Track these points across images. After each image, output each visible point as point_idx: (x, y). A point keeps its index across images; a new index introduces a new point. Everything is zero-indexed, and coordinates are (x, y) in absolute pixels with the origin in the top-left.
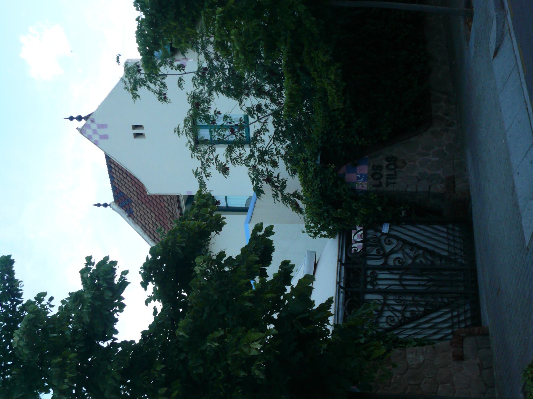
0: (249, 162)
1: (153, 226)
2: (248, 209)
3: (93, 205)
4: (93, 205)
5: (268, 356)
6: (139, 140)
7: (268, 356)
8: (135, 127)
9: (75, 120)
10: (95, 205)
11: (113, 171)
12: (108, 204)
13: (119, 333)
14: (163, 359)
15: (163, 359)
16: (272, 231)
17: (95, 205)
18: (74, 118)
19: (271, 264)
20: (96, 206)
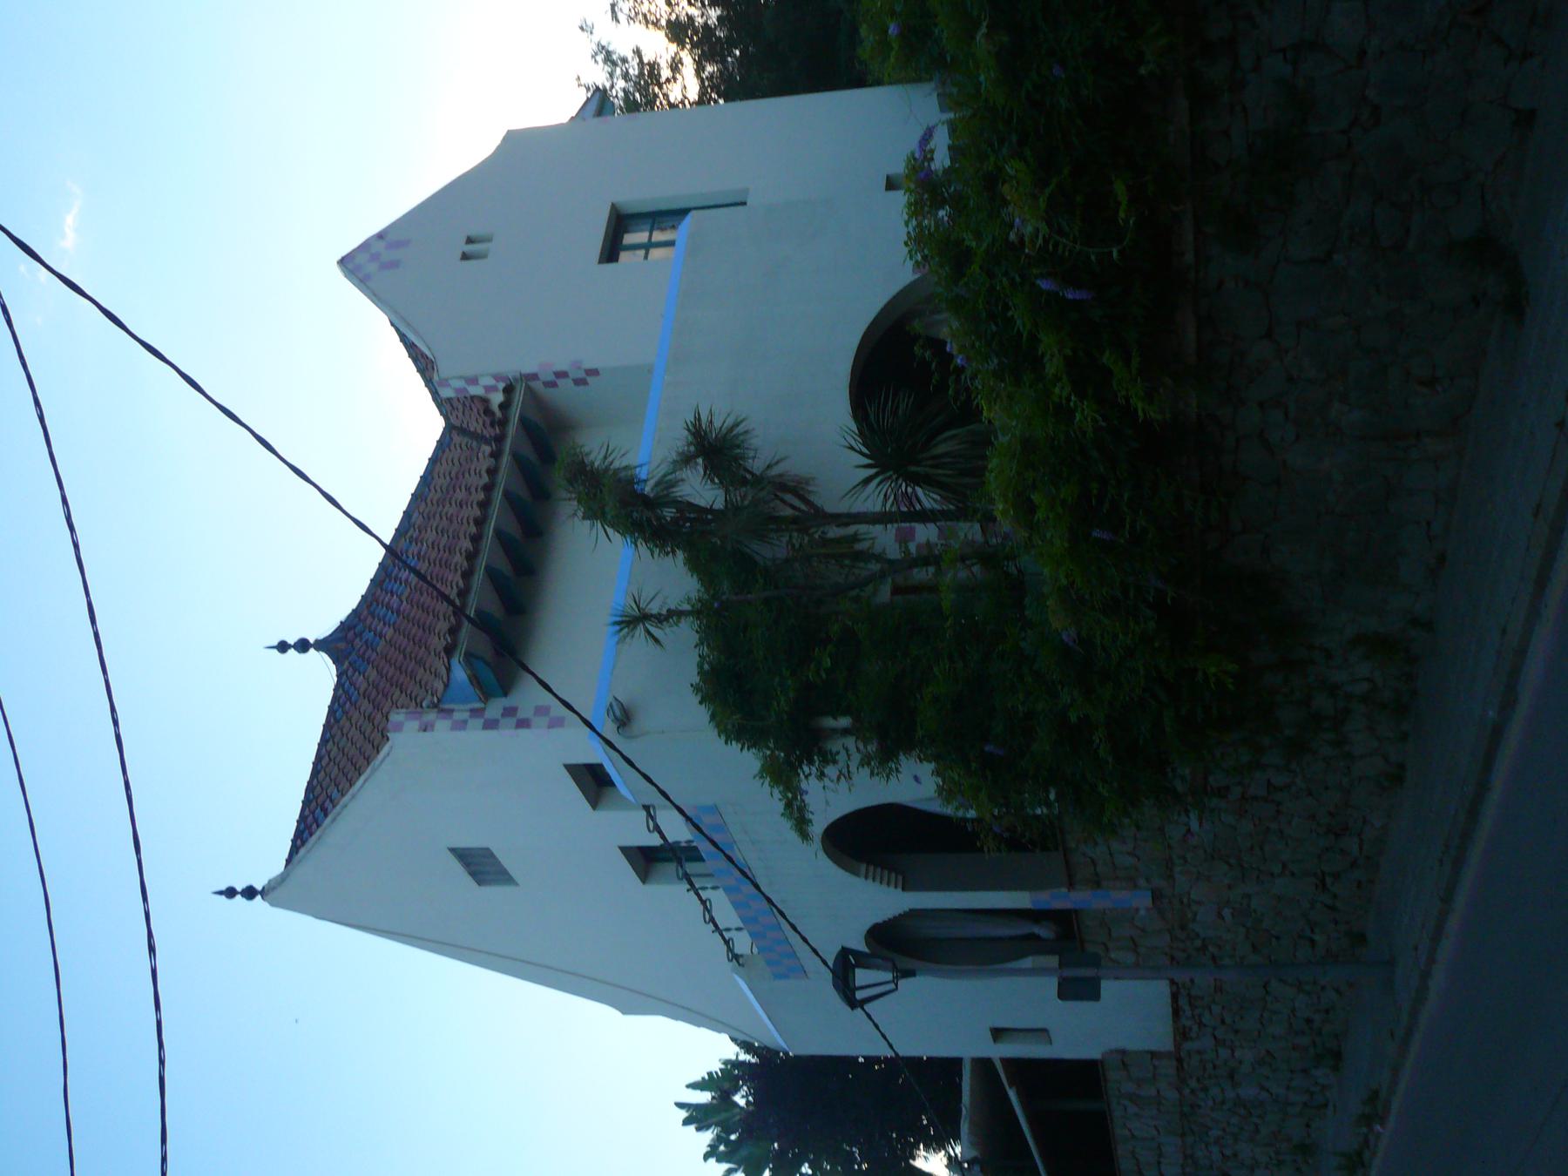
6: (473, 233)
8: (470, 241)
10: (220, 893)
17: (220, 893)
20: (223, 897)
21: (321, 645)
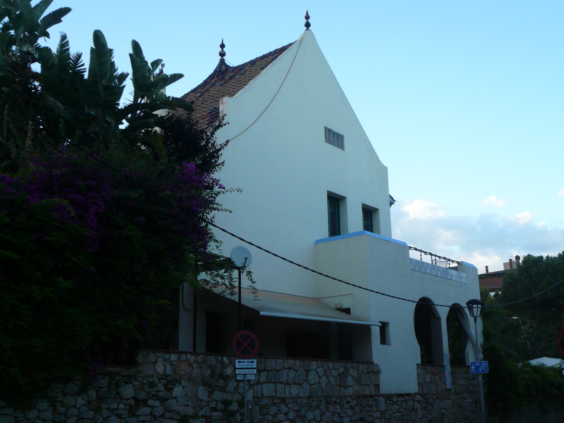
0: (209, 213)
1: (227, 94)
2: (377, 234)
3: (307, 11)
4: (307, 11)
5: (201, 263)
7: (201, 263)
9: (220, 49)
10: (307, 14)
11: (215, 78)
12: (310, 28)
13: (97, 29)
14: (71, 71)
15: (71, 71)
16: (481, 300)
17: (307, 14)
18: (223, 49)
19: (466, 302)
20: (305, 14)
21: (222, 62)
